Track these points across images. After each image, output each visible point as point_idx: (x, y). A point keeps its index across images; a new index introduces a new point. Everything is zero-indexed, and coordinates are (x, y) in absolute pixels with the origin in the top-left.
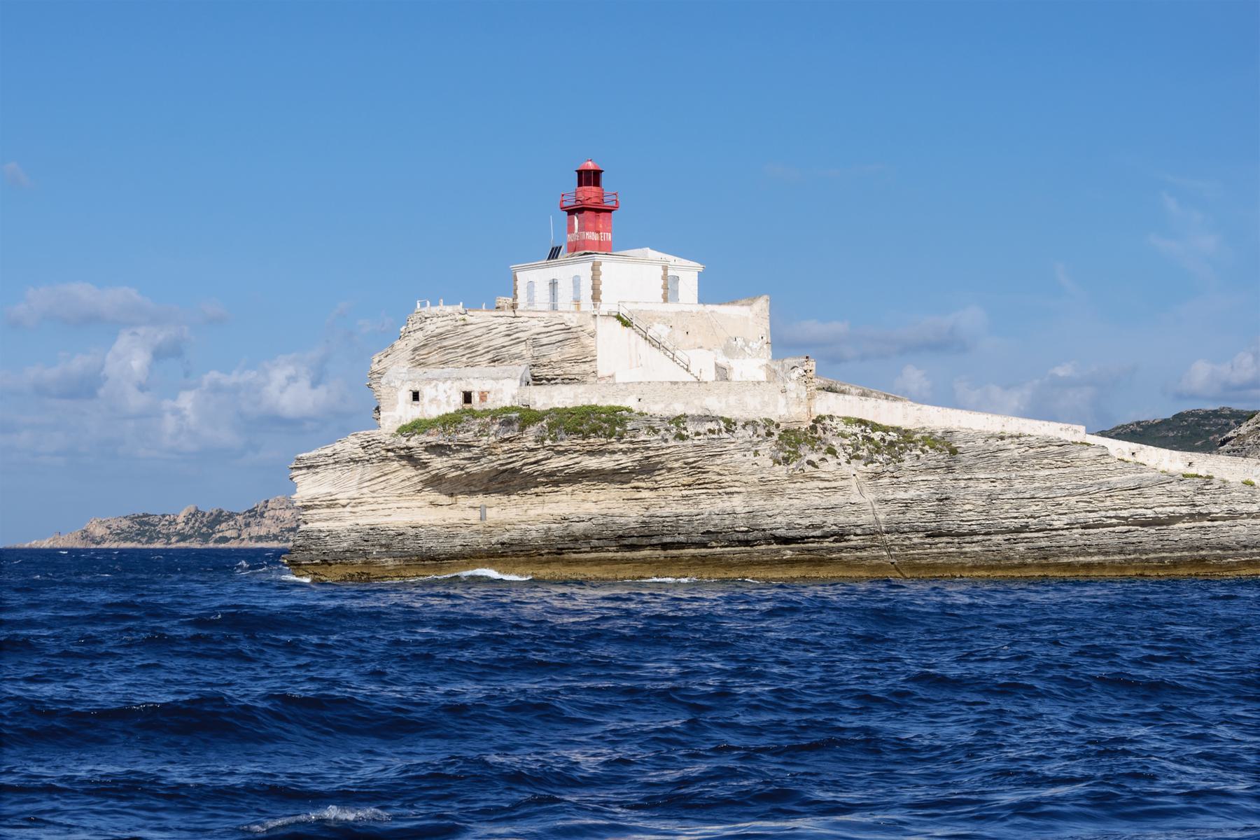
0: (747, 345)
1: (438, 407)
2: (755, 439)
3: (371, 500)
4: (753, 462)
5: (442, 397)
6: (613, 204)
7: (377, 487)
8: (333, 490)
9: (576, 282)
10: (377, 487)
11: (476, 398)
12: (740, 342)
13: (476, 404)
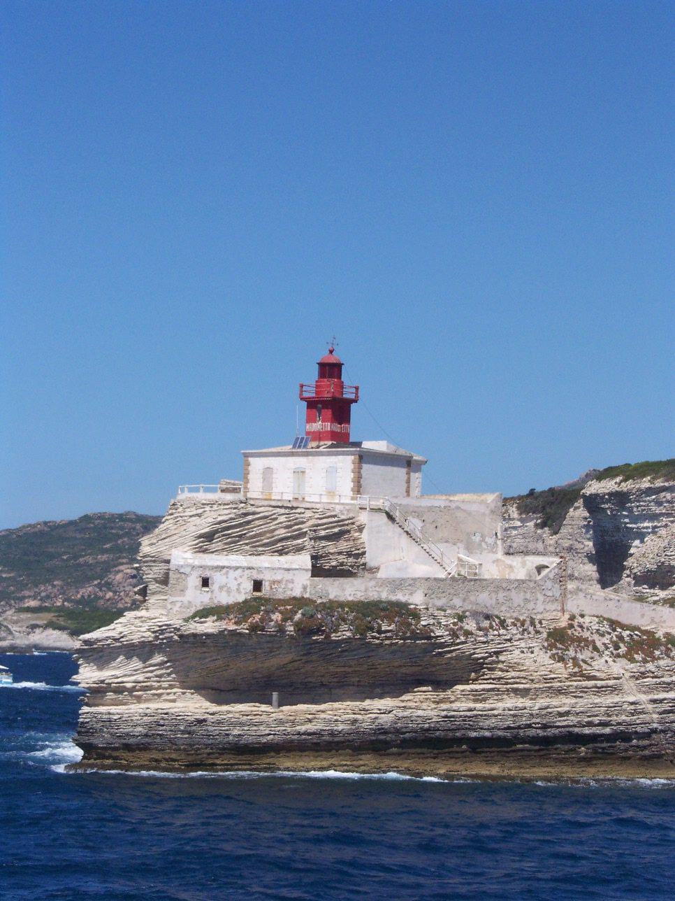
0: (483, 540)
3: (156, 685)
4: (534, 659)
6: (353, 396)
11: (266, 587)
13: (266, 590)
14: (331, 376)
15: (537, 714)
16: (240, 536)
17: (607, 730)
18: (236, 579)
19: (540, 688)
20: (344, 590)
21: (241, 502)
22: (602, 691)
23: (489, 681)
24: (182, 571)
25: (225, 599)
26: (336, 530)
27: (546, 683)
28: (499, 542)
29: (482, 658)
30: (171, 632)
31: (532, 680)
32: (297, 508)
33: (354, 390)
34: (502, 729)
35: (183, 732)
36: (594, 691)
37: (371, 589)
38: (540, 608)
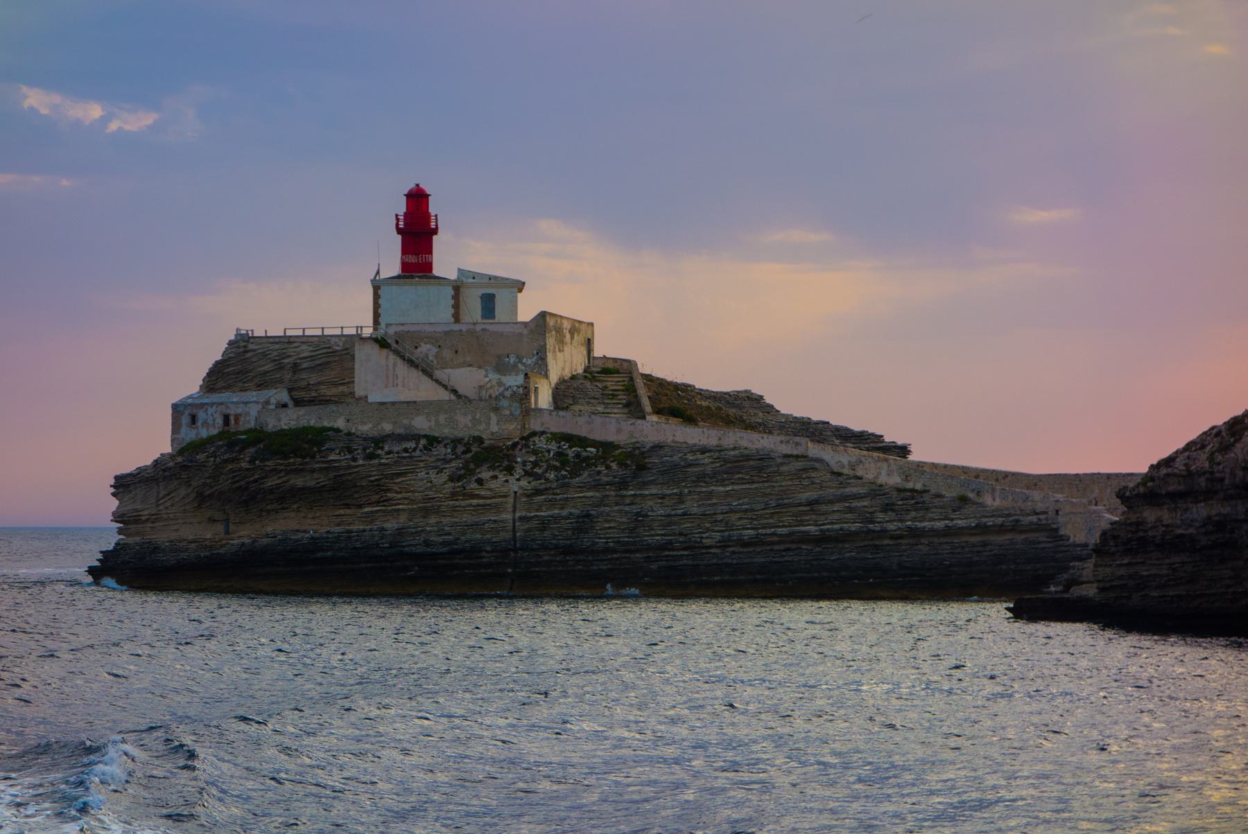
0: (520, 362)
12: (512, 360)
20: (279, 420)
38: (494, 428)
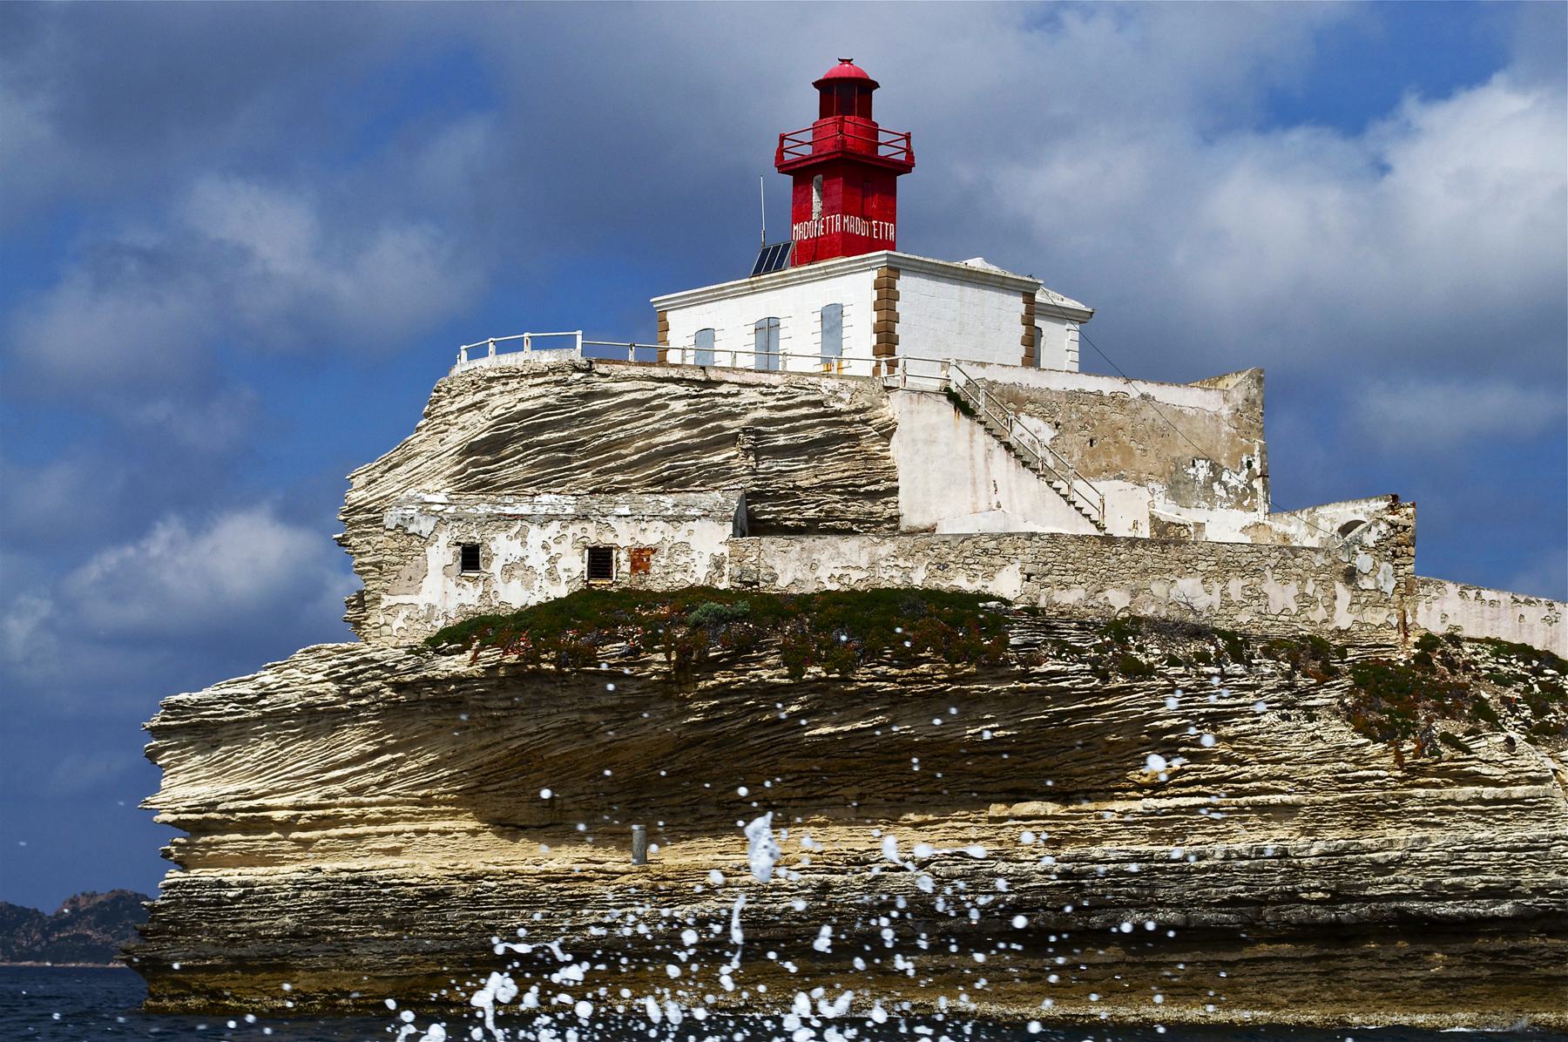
1: (528, 586)
2: (1300, 681)
5: (538, 560)
7: (366, 780)
8: (254, 785)
9: (832, 319)
10: (366, 780)
11: (622, 566)
14: (846, 109)
15: (1314, 868)
16: (570, 448)
17: (1506, 908)
18: (545, 547)
19: (1326, 803)
20: (813, 567)
21: (577, 369)
22: (1497, 811)
23: (1192, 789)
24: (412, 529)
25: (515, 596)
26: (817, 434)
27: (1342, 790)
28: (1258, 484)
29: (1173, 729)
30: (374, 678)
31: (1307, 783)
32: (721, 383)
33: (903, 144)
34: (1217, 905)
35: (387, 924)
36: (1473, 811)
37: (884, 564)
38: (1343, 620)
